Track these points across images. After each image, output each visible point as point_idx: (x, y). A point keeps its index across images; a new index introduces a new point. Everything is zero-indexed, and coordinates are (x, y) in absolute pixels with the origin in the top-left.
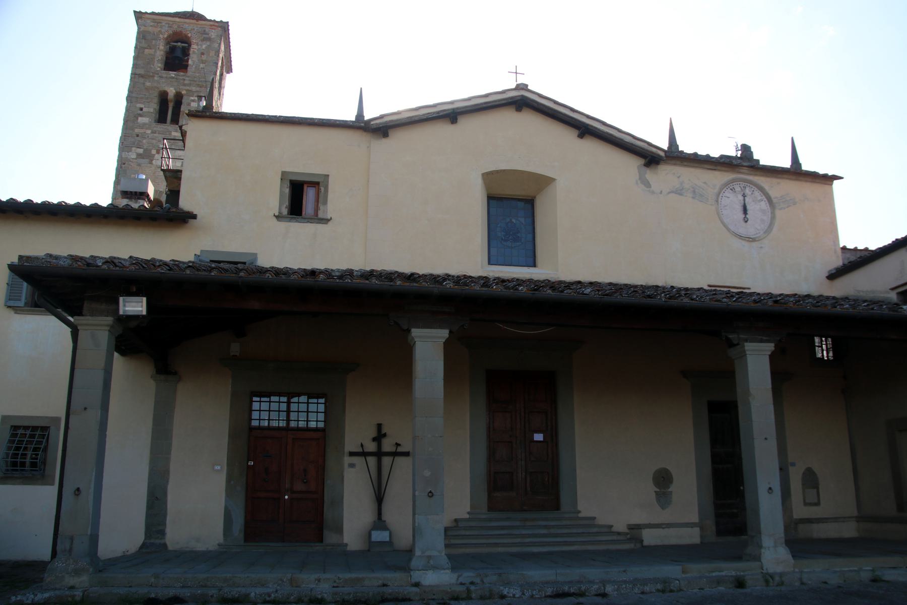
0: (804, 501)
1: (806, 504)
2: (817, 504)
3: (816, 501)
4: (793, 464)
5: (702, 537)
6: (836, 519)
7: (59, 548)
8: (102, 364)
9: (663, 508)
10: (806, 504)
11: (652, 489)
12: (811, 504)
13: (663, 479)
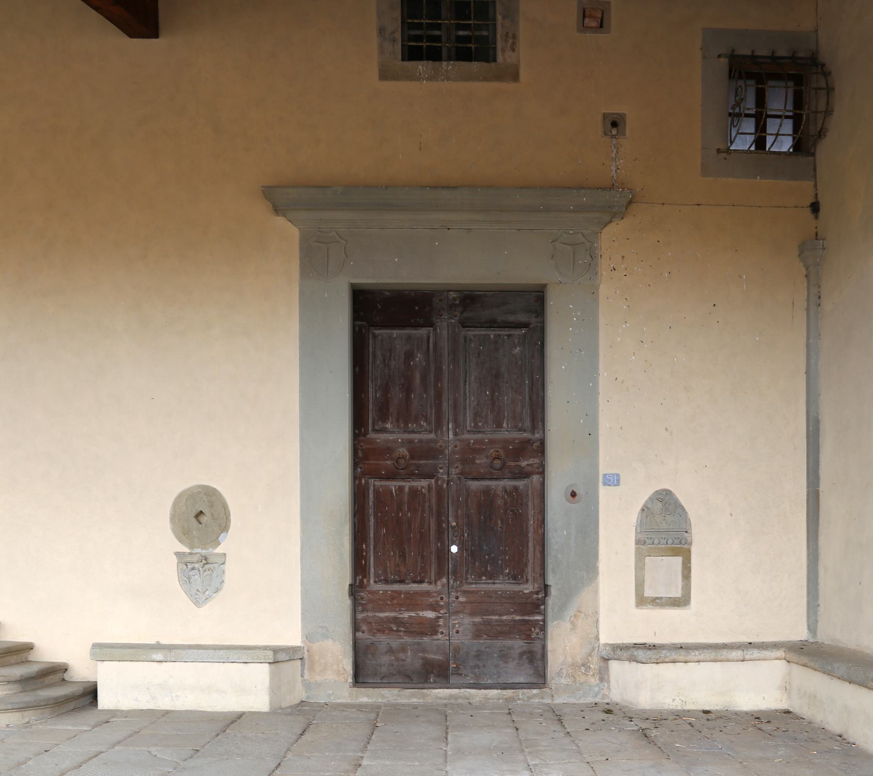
0: (640, 585)
1: (642, 601)
2: (682, 602)
3: (676, 592)
4: (613, 481)
5: (275, 689)
6: (715, 651)
7: (287, 658)
8: (195, 651)
9: (199, 598)
10: (642, 601)
11: (168, 545)
12: (657, 602)
13: (201, 518)
